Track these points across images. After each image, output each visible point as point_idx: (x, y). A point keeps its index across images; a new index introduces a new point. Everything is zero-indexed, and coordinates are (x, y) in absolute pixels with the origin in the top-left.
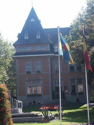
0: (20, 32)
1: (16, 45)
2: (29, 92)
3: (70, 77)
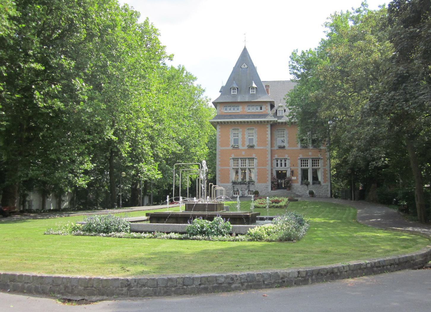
0: (224, 84)
1: (218, 103)
2: (73, 63)
3: (301, 156)
